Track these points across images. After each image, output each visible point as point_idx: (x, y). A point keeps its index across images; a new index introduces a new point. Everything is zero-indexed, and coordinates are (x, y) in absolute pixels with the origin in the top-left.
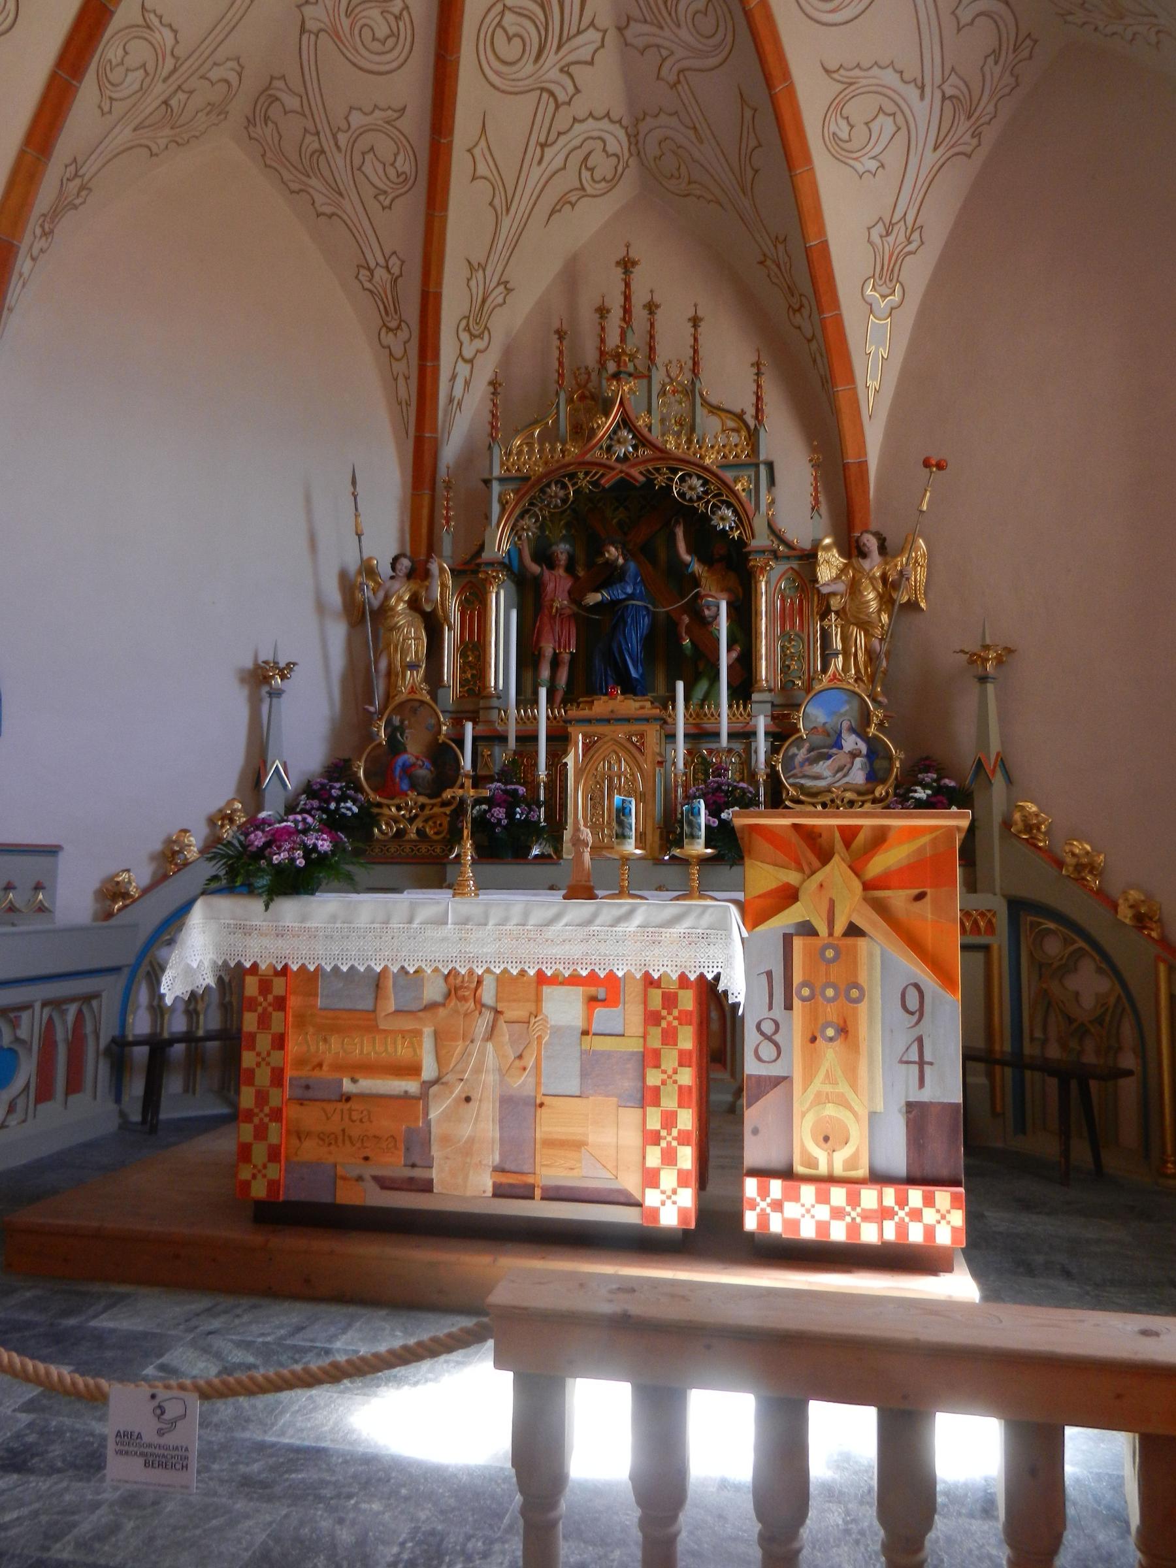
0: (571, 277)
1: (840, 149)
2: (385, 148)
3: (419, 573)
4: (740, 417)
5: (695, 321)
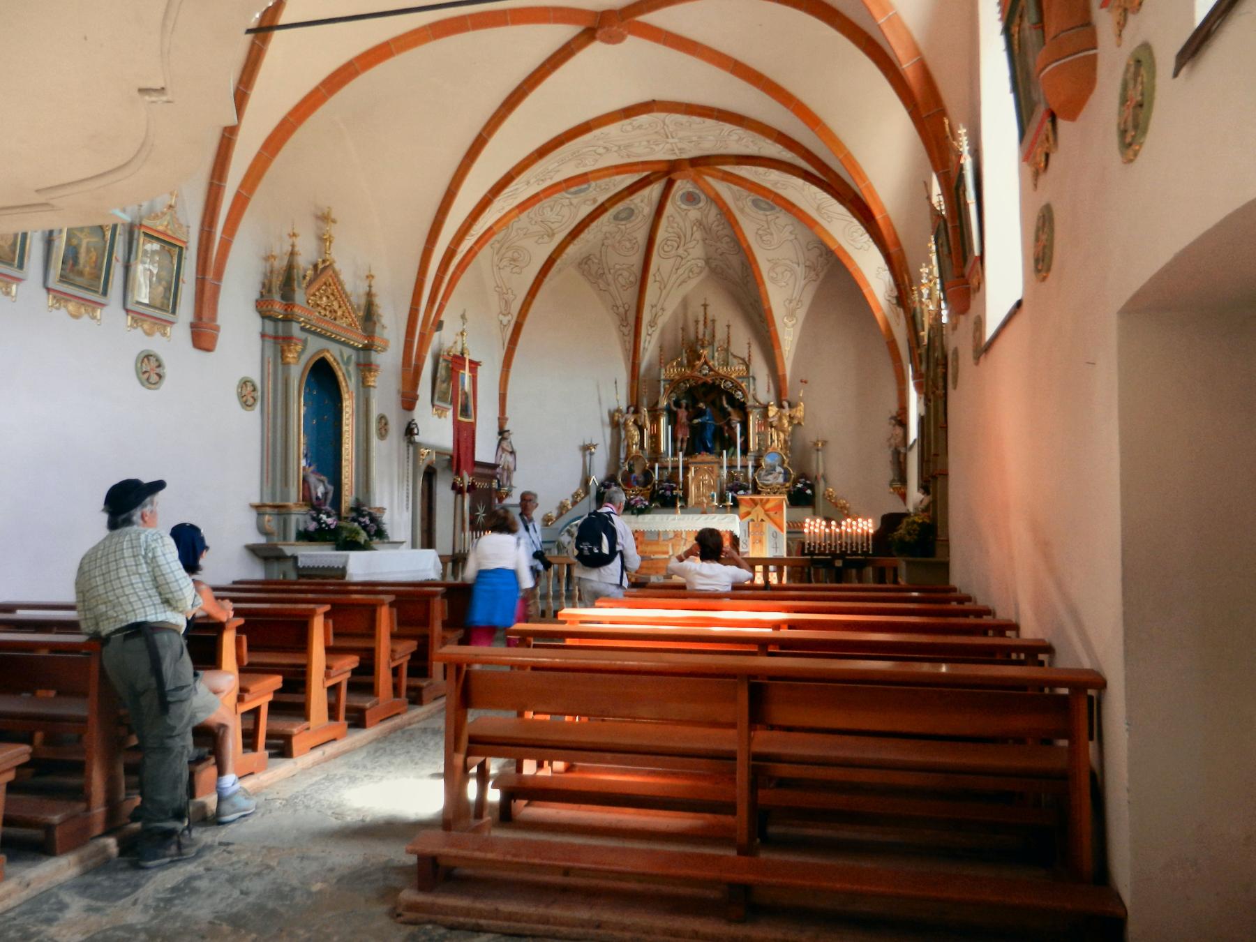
0: (685, 303)
1: (774, 280)
2: (626, 274)
3: (637, 411)
4: (743, 359)
5: (729, 326)
